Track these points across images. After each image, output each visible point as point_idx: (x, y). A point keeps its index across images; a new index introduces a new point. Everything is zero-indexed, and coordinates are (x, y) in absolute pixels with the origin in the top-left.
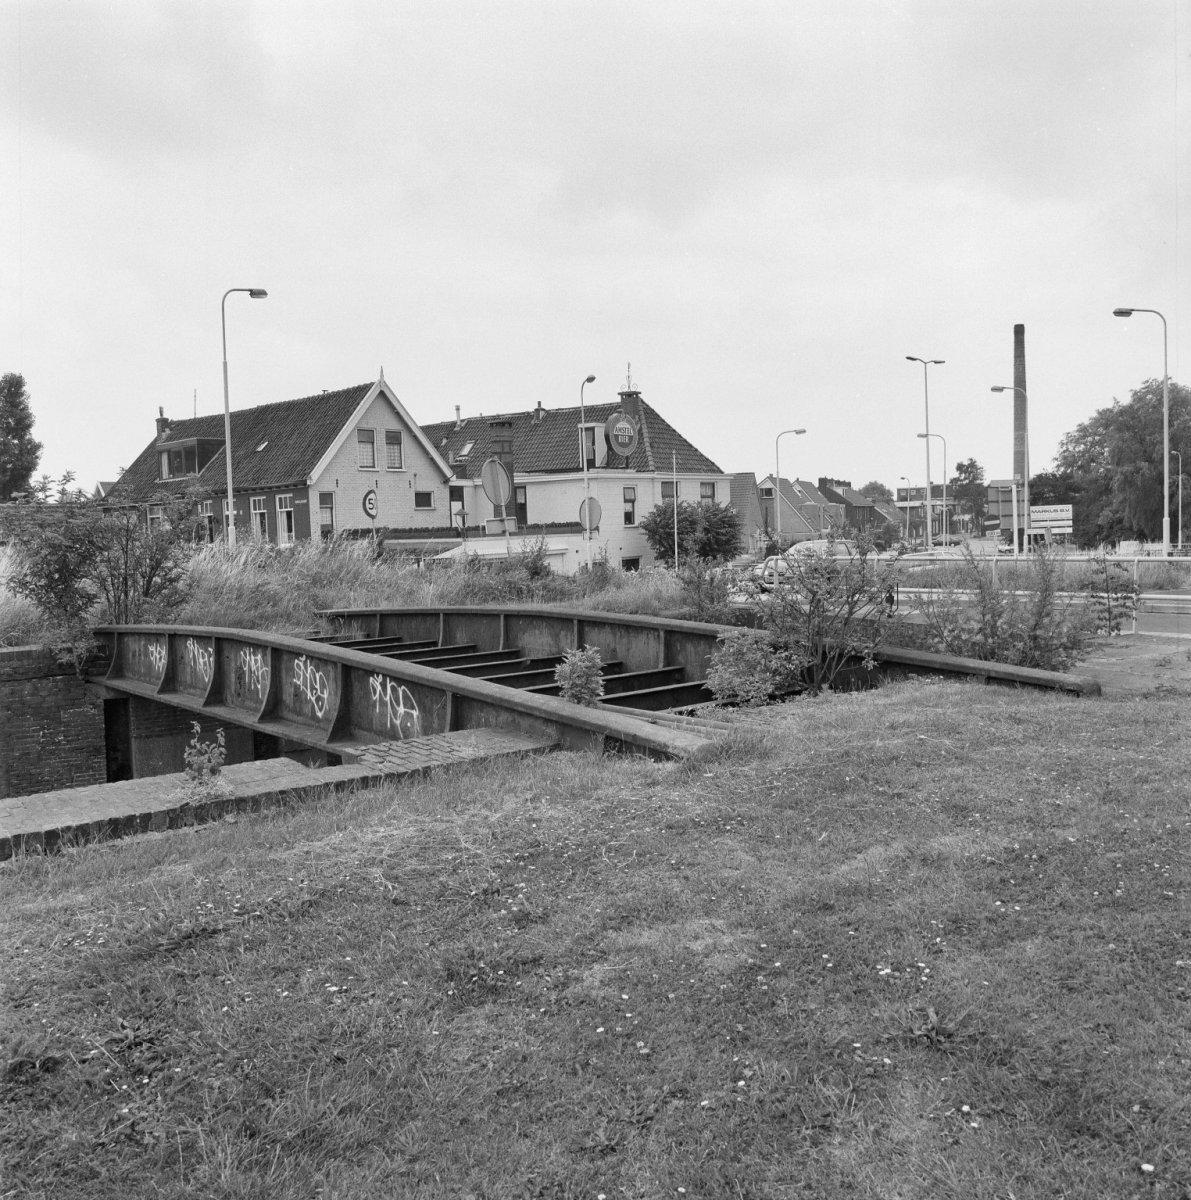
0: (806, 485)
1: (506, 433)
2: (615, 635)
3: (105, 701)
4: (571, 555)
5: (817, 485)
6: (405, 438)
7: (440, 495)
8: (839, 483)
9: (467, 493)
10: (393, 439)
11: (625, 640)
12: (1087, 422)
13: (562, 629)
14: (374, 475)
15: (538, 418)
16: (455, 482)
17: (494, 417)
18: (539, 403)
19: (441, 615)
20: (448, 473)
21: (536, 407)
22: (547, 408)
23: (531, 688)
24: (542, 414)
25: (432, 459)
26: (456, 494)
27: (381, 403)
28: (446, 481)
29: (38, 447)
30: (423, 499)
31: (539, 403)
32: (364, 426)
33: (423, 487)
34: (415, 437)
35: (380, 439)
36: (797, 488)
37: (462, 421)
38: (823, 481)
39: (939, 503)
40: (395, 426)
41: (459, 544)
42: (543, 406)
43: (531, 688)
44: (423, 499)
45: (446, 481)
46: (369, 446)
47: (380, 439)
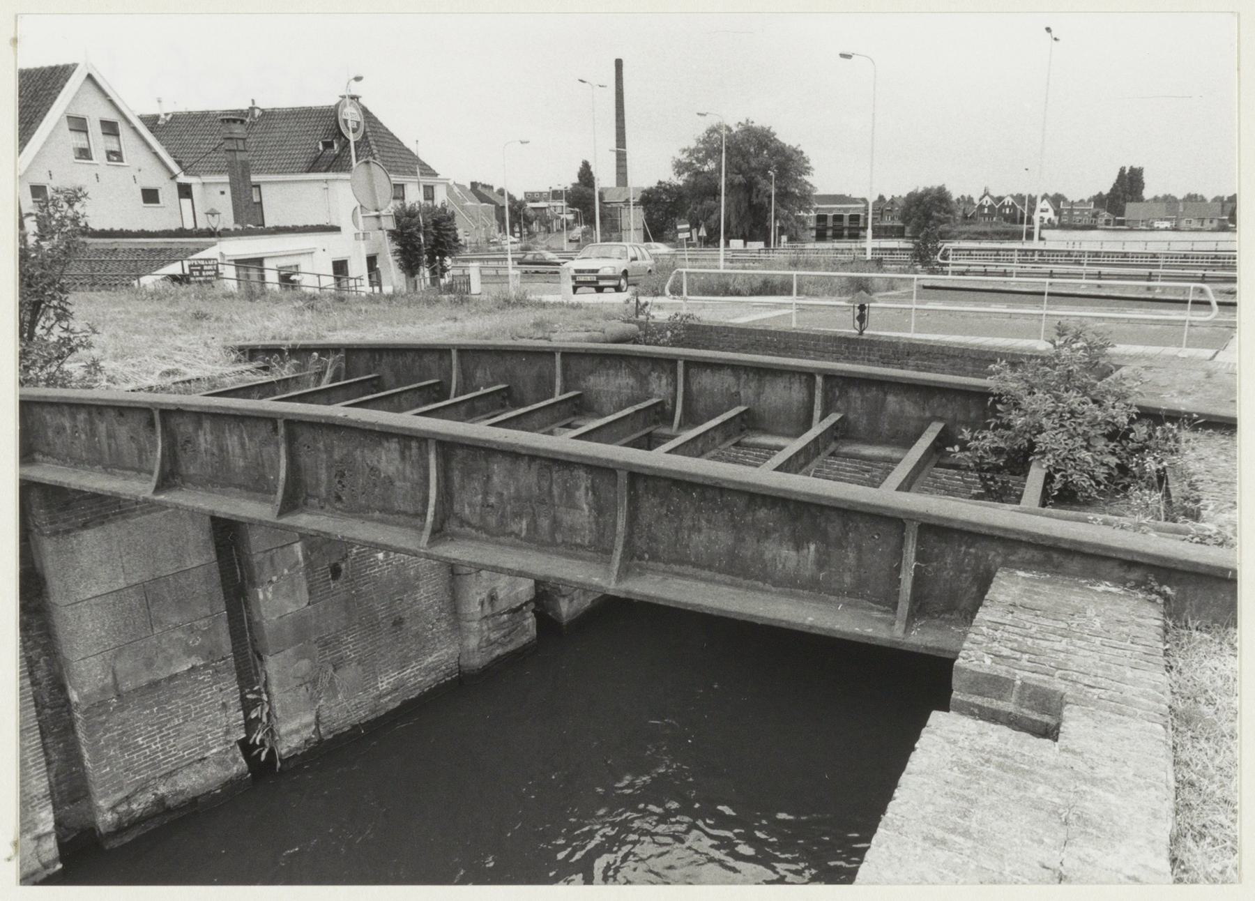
0: (462, 187)
1: (238, 130)
2: (739, 379)
3: (1056, 740)
4: (319, 253)
5: (469, 187)
6: (122, 127)
7: (168, 193)
8: (485, 186)
9: (196, 191)
10: (110, 128)
11: (753, 385)
12: (804, 155)
13: (653, 370)
14: (93, 168)
15: (253, 115)
16: (182, 179)
17: (225, 113)
18: (253, 101)
19: (454, 353)
20: (176, 169)
21: (251, 105)
22: (262, 107)
23: (488, 415)
24: (257, 112)
25: (156, 154)
26: (185, 191)
27: (90, 87)
28: (174, 177)
29: (660, 183)
30: (150, 196)
31: (253, 101)
32: (74, 113)
33: (151, 185)
34: (134, 129)
35: (95, 129)
36: (456, 190)
37: (166, 114)
38: (474, 185)
39: (559, 204)
40: (111, 116)
41: (213, 244)
42: (257, 105)
43: (625, 441)
44: (150, 196)
45: (174, 177)
46: (84, 135)
47: (95, 129)
